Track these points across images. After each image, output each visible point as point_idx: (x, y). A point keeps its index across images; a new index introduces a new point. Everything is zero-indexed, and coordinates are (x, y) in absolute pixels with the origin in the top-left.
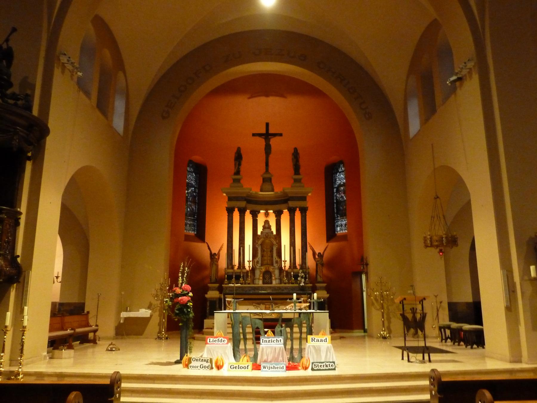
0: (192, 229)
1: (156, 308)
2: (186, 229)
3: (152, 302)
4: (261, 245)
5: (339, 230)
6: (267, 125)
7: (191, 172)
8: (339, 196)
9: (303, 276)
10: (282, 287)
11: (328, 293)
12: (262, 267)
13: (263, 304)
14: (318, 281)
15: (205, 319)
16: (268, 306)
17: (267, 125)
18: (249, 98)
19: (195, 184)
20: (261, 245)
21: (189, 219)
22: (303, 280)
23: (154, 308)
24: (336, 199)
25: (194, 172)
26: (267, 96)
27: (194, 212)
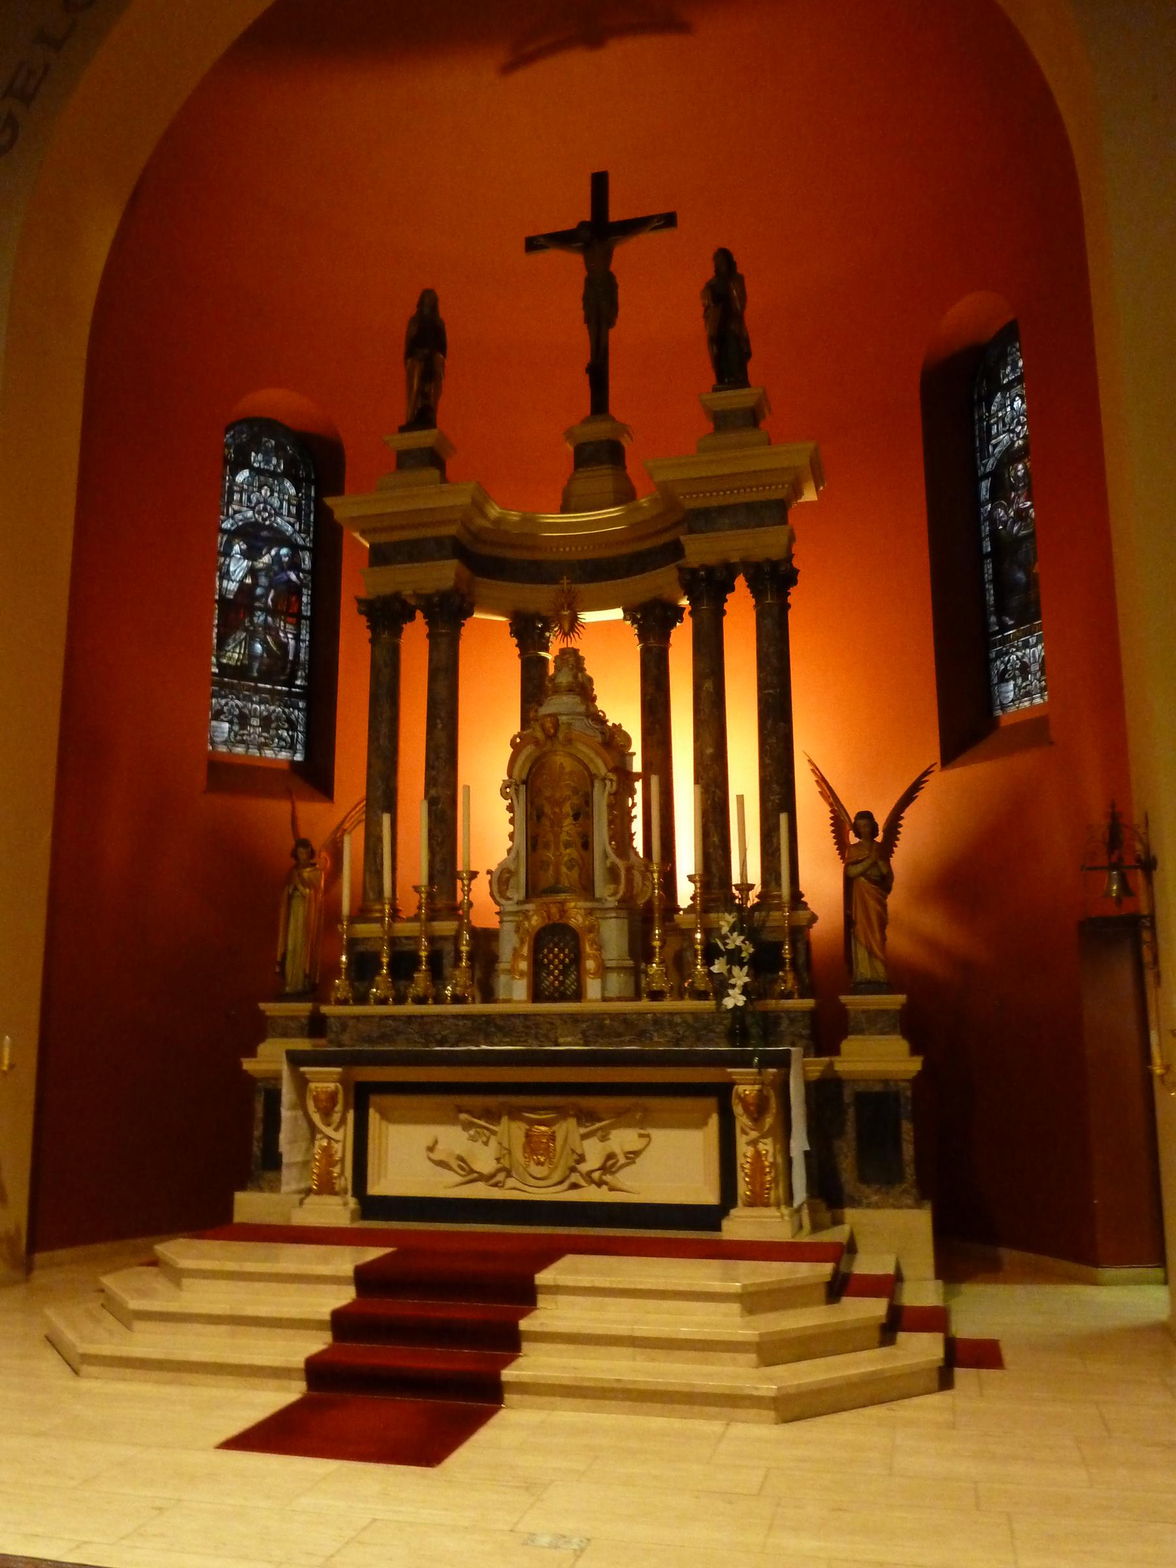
0: (281, 738)
2: (243, 742)
4: (524, 782)
5: (1011, 695)
6: (600, 182)
7: (273, 474)
8: (1006, 513)
9: (739, 949)
10: (641, 1014)
11: (914, 1051)
12: (530, 907)
13: (515, 1114)
14: (859, 979)
15: (243, 1188)
16: (543, 1128)
17: (600, 182)
18: (508, 69)
19: (295, 531)
20: (524, 782)
21: (258, 691)
22: (741, 977)
24: (994, 533)
25: (286, 474)
26: (594, 40)
27: (291, 658)
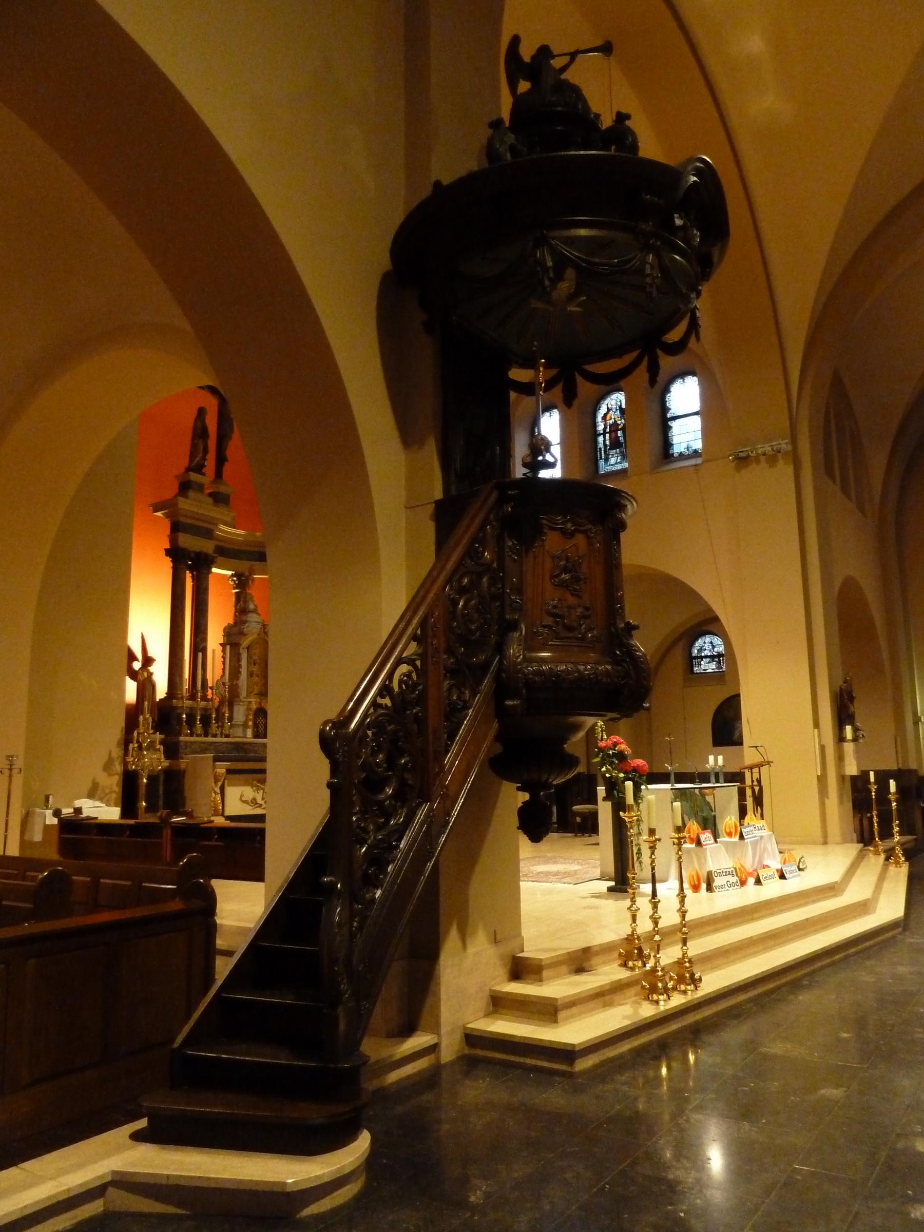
1: (109, 796)
3: (98, 780)
4: (248, 648)
23: (102, 795)
